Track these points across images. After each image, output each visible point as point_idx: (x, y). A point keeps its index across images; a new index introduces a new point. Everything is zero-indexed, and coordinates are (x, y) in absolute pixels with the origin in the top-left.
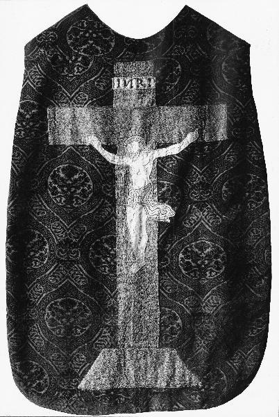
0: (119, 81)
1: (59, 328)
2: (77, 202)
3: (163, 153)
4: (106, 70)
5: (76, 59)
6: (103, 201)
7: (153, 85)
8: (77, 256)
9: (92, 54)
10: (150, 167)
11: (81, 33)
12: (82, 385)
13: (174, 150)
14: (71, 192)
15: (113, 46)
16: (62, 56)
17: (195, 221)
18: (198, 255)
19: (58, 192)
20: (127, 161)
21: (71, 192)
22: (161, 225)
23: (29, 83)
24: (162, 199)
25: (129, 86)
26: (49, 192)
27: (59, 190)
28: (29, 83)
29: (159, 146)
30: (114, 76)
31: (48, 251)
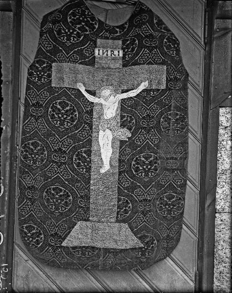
0: (99, 50)
1: (56, 120)
2: (67, 124)
3: (125, 96)
4: (91, 43)
5: (73, 32)
6: (84, 126)
7: (121, 55)
8: (65, 159)
9: (83, 32)
10: (116, 104)
11: (77, 17)
12: (64, 244)
13: (132, 94)
14: (70, 33)
15: (97, 28)
16: (64, 29)
17: (143, 140)
18: (144, 162)
19: (55, 117)
20: (102, 101)
21: (70, 33)
22: (122, 142)
23: (33, 213)
24: (123, 125)
25: (105, 55)
26: (49, 117)
27: (56, 116)
28: (33, 213)
29: (123, 92)
30: (96, 47)
31: (43, 239)
